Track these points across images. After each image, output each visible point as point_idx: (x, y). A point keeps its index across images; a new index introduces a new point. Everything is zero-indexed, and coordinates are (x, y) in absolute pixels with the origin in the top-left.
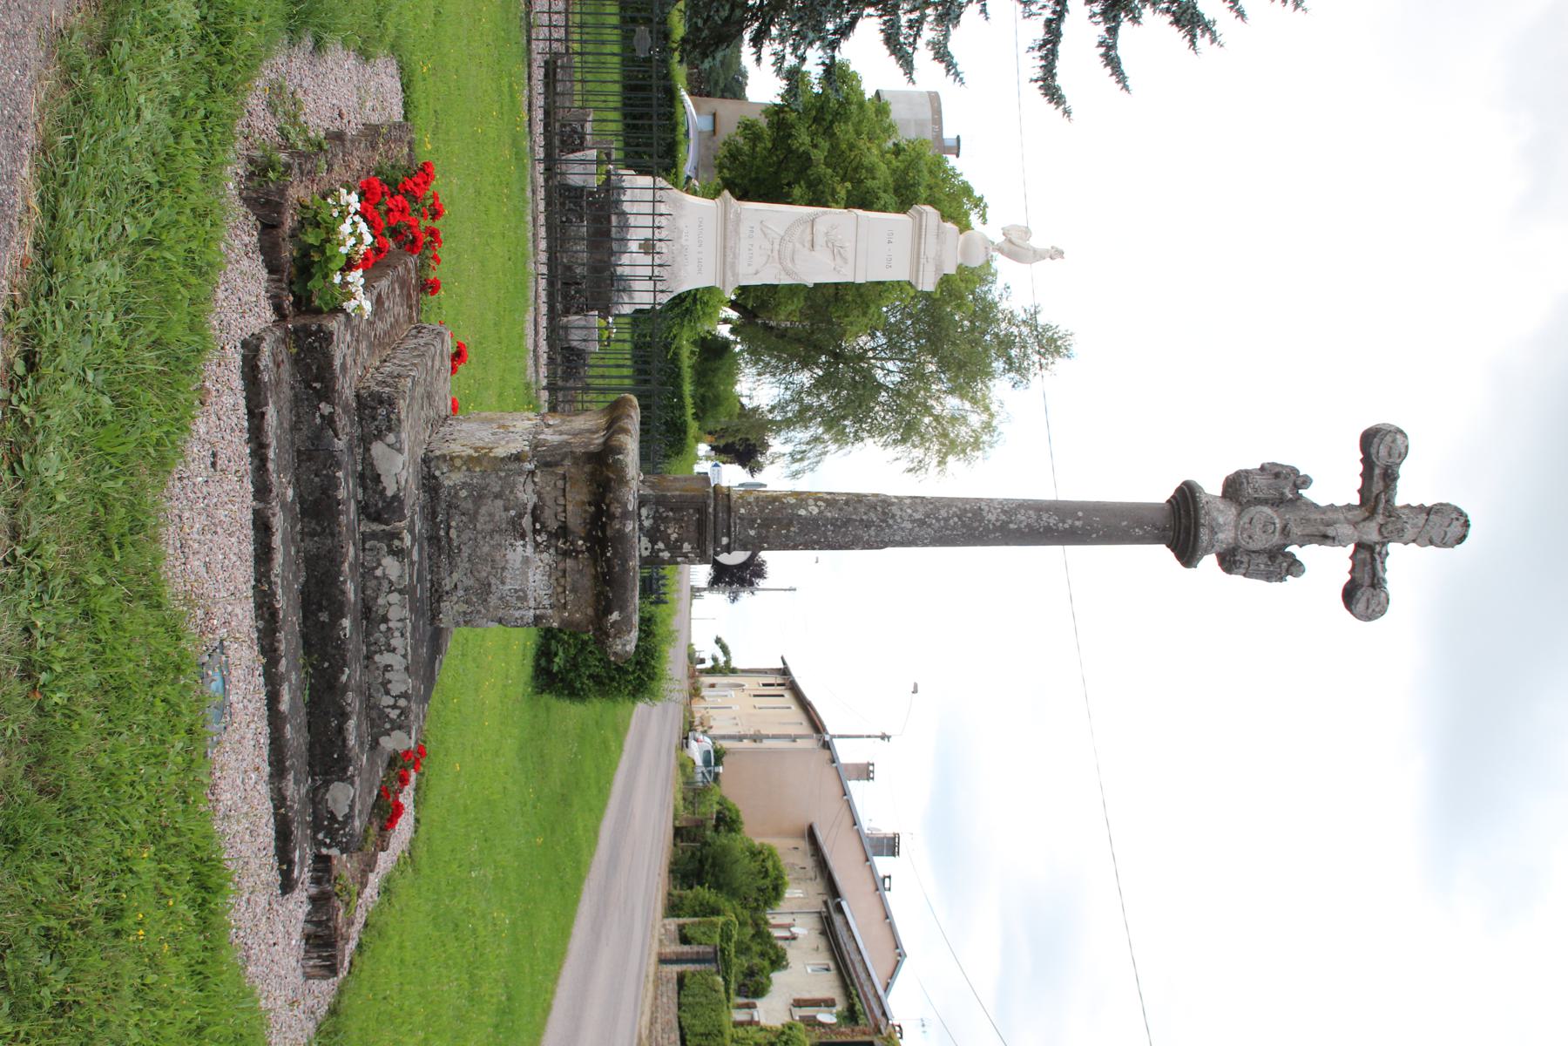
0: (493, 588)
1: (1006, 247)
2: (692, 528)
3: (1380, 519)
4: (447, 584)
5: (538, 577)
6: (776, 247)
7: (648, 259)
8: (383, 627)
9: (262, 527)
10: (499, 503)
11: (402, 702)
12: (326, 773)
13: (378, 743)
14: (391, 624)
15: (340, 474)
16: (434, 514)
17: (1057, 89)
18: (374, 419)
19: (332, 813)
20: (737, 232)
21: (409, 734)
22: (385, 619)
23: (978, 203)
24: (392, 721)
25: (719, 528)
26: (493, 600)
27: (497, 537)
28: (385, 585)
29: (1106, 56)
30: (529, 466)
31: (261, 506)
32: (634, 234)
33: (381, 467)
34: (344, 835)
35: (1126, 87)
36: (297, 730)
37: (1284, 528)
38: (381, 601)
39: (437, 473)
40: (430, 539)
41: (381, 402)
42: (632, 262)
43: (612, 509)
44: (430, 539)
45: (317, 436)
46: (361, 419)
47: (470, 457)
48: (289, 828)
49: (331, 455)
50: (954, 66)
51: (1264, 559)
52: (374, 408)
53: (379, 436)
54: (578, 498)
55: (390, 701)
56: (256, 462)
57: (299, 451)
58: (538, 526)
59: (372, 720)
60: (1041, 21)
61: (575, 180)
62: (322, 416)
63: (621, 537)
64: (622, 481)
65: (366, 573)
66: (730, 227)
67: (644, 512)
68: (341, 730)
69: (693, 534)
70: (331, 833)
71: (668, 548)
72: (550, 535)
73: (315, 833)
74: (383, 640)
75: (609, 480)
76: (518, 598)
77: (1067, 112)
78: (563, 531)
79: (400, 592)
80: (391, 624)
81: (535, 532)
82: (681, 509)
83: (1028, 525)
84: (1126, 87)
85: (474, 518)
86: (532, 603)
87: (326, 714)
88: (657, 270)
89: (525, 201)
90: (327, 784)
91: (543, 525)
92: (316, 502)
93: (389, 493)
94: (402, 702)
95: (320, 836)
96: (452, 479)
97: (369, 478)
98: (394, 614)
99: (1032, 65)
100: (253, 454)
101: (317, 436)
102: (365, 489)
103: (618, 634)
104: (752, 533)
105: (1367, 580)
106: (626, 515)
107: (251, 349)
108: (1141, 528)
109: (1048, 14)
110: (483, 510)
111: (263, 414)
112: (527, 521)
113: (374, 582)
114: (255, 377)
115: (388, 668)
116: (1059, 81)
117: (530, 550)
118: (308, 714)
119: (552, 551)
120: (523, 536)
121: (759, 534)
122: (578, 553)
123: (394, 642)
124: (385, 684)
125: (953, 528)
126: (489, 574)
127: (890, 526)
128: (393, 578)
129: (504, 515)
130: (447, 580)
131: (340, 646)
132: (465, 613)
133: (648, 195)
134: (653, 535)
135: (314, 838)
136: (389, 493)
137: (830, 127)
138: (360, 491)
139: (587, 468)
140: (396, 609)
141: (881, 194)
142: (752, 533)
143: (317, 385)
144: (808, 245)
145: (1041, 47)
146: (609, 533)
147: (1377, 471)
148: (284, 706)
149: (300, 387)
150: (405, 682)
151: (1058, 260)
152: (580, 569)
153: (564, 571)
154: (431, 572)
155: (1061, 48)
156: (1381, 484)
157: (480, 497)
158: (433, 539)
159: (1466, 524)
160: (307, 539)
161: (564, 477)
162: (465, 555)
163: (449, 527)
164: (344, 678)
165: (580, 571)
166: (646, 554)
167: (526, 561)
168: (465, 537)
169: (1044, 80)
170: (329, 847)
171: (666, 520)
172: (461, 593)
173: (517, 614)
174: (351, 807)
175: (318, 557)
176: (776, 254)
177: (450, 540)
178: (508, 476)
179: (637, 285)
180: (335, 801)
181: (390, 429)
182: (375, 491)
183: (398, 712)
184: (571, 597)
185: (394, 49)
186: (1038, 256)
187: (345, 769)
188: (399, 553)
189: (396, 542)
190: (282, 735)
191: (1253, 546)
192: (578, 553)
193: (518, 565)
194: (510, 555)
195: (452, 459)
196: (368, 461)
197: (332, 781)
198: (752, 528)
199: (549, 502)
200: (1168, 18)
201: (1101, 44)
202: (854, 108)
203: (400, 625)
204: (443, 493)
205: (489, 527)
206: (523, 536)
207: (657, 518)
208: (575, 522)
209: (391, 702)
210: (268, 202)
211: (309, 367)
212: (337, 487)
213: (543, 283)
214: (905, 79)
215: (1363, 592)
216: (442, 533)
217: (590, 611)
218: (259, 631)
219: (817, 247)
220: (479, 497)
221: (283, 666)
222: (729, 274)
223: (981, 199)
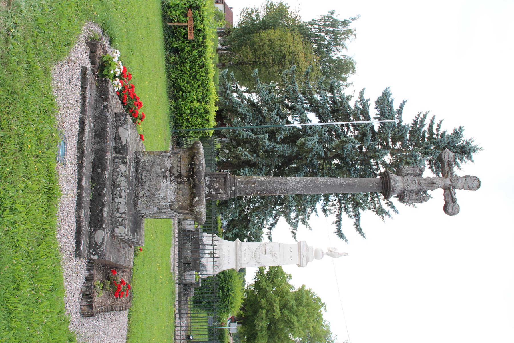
0: (156, 196)
1: (329, 252)
2: (222, 184)
3: (450, 177)
4: (141, 194)
5: (171, 192)
6: (254, 254)
7: (212, 259)
8: (118, 189)
9: (82, 122)
10: (159, 167)
11: (123, 216)
12: (95, 226)
13: (114, 231)
14: (121, 188)
15: (108, 124)
16: (137, 170)
17: (342, 234)
18: (120, 120)
19: (96, 242)
20: (241, 250)
21: (125, 227)
22: (119, 186)
23: (323, 305)
24: (119, 222)
25: (231, 183)
26: (156, 200)
27: (158, 178)
28: (120, 174)
29: (356, 228)
30: (169, 154)
31: (82, 116)
32: (207, 252)
33: (121, 135)
34: (100, 251)
35: (364, 237)
36: (87, 179)
37: (419, 182)
38: (118, 180)
39: (139, 157)
40: (136, 178)
41: (123, 115)
42: (207, 260)
43: (196, 162)
44: (136, 178)
45: (102, 112)
46: (116, 120)
47: (150, 152)
48: (81, 229)
49: (106, 118)
50: (309, 225)
51: (414, 194)
52: (120, 117)
53: (121, 125)
54: (185, 164)
55: (119, 215)
56: (82, 102)
57: (96, 116)
58: (171, 174)
59: (112, 222)
60: (335, 215)
61: (188, 227)
62: (104, 106)
63: (198, 171)
64: (199, 152)
65: (114, 170)
66: (238, 248)
67: (207, 178)
68: (101, 210)
69: (223, 187)
70: (95, 250)
71: (214, 191)
72: (176, 177)
73: (90, 249)
74: (118, 193)
75: (195, 153)
76: (164, 199)
77: (346, 241)
78: (180, 176)
79: (125, 176)
80: (121, 188)
81: (171, 176)
82: (218, 177)
83: (334, 183)
84: (364, 237)
85: (150, 172)
86: (169, 201)
87: (97, 204)
88: (215, 259)
89: (170, 227)
90: (95, 230)
91: (173, 174)
92: (100, 132)
93: (123, 144)
94: (123, 216)
95: (91, 251)
96: (144, 159)
97: (117, 139)
98: (122, 184)
99: (334, 228)
100: (81, 99)
101: (102, 112)
102: (116, 142)
103: (198, 205)
104: (243, 186)
105: (450, 200)
106: (200, 164)
107: (84, 70)
108: (371, 183)
109: (337, 213)
110: (154, 169)
111: (86, 88)
112: (168, 173)
113: (117, 173)
114: (85, 77)
115: (119, 203)
116: (342, 232)
117: (168, 182)
118: (91, 204)
119: (176, 183)
120: (166, 178)
121: (245, 186)
122: (184, 182)
123: (122, 194)
124: (118, 209)
125: (309, 184)
126: (155, 191)
127: (288, 183)
128: (123, 172)
129: (160, 171)
130: (141, 193)
131: (104, 180)
132: (146, 204)
133: (211, 239)
134: (210, 187)
135: (89, 251)
136: (123, 144)
137: (272, 280)
138: (114, 143)
139: (188, 154)
140: (123, 182)
141: (290, 300)
142: (243, 186)
143: (103, 97)
144: (264, 253)
145: (336, 223)
146: (195, 171)
147: (446, 164)
148: (83, 183)
149: (98, 97)
150: (124, 208)
151: (346, 256)
152: (185, 188)
153: (180, 189)
154: (136, 190)
155: (342, 222)
156: (448, 168)
157: (153, 165)
158: (137, 179)
159: (479, 181)
160: (96, 144)
161: (180, 158)
162: (147, 184)
163: (142, 175)
164: (104, 192)
165: (185, 188)
166: (207, 193)
167: (167, 186)
168: (147, 178)
169: (337, 232)
170: (94, 255)
171: (214, 181)
172: (145, 197)
173: (164, 204)
174: (103, 240)
175: (99, 150)
176: (253, 256)
177: (142, 179)
178: (162, 158)
179: (208, 268)
180: (97, 238)
181: (125, 123)
182: (119, 143)
183: (121, 219)
184: (182, 197)
185: (130, 311)
186: (340, 255)
187: (102, 225)
188: (125, 163)
189: (125, 160)
190: (82, 194)
191: (410, 189)
192: (184, 182)
193: (164, 188)
194: (162, 184)
195: (144, 152)
196: (117, 134)
197: (97, 230)
198: (242, 184)
199: (175, 166)
200: (375, 213)
201: (355, 224)
202: (280, 273)
203: (124, 188)
204: (141, 164)
205: (155, 175)
206: (166, 178)
207: (211, 181)
208: (184, 172)
209: (119, 215)
210: (93, 44)
211: (101, 91)
212: (107, 128)
213: (177, 248)
214: (294, 240)
215: (450, 206)
216: (140, 177)
217: (188, 202)
218: (78, 157)
219: (267, 254)
220: (152, 165)
221: (84, 170)
222: (238, 263)
223: (324, 304)
